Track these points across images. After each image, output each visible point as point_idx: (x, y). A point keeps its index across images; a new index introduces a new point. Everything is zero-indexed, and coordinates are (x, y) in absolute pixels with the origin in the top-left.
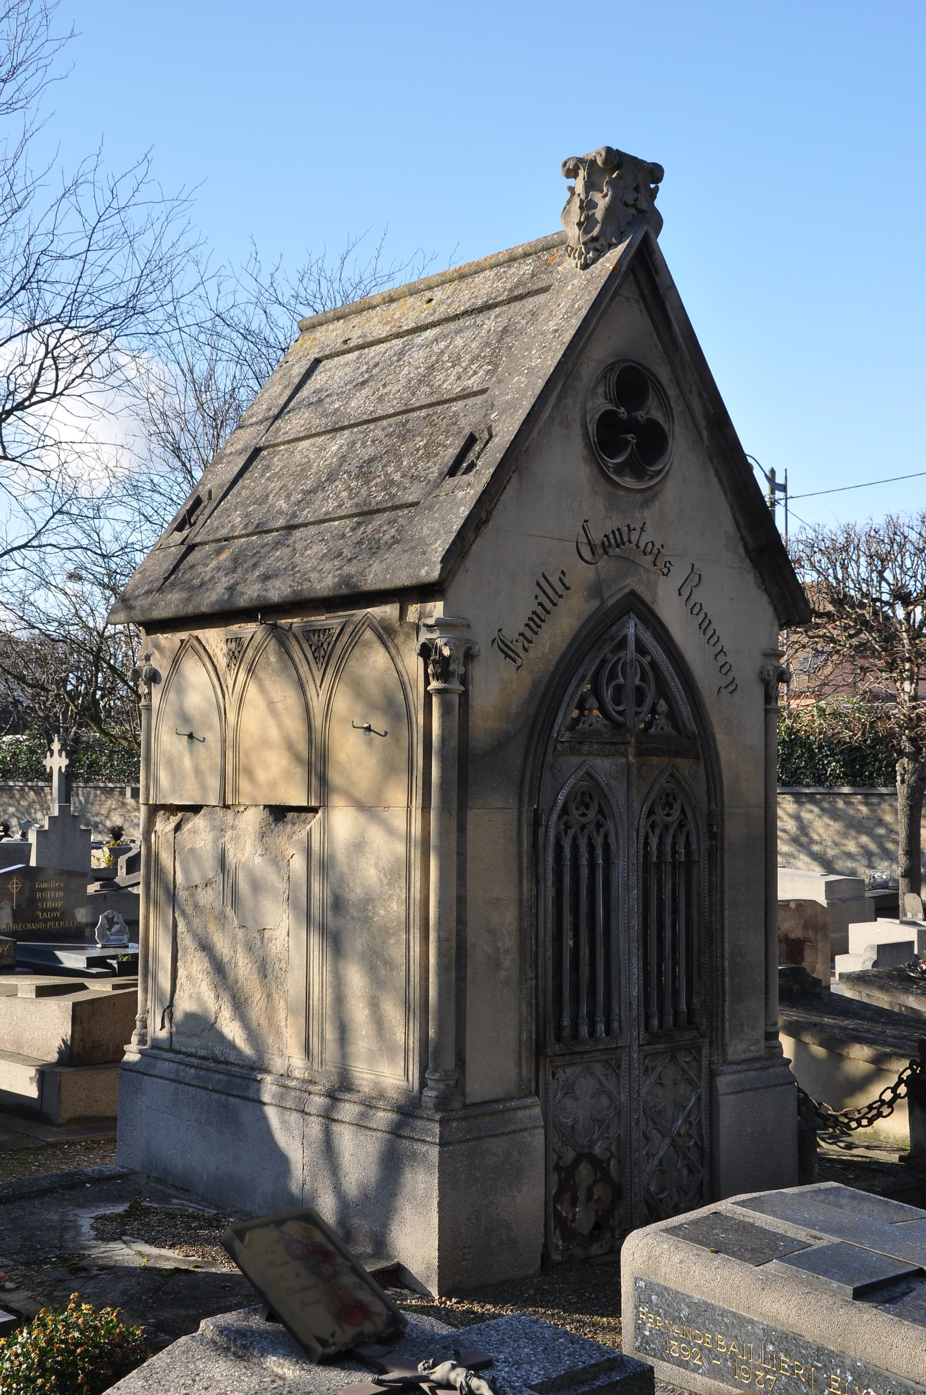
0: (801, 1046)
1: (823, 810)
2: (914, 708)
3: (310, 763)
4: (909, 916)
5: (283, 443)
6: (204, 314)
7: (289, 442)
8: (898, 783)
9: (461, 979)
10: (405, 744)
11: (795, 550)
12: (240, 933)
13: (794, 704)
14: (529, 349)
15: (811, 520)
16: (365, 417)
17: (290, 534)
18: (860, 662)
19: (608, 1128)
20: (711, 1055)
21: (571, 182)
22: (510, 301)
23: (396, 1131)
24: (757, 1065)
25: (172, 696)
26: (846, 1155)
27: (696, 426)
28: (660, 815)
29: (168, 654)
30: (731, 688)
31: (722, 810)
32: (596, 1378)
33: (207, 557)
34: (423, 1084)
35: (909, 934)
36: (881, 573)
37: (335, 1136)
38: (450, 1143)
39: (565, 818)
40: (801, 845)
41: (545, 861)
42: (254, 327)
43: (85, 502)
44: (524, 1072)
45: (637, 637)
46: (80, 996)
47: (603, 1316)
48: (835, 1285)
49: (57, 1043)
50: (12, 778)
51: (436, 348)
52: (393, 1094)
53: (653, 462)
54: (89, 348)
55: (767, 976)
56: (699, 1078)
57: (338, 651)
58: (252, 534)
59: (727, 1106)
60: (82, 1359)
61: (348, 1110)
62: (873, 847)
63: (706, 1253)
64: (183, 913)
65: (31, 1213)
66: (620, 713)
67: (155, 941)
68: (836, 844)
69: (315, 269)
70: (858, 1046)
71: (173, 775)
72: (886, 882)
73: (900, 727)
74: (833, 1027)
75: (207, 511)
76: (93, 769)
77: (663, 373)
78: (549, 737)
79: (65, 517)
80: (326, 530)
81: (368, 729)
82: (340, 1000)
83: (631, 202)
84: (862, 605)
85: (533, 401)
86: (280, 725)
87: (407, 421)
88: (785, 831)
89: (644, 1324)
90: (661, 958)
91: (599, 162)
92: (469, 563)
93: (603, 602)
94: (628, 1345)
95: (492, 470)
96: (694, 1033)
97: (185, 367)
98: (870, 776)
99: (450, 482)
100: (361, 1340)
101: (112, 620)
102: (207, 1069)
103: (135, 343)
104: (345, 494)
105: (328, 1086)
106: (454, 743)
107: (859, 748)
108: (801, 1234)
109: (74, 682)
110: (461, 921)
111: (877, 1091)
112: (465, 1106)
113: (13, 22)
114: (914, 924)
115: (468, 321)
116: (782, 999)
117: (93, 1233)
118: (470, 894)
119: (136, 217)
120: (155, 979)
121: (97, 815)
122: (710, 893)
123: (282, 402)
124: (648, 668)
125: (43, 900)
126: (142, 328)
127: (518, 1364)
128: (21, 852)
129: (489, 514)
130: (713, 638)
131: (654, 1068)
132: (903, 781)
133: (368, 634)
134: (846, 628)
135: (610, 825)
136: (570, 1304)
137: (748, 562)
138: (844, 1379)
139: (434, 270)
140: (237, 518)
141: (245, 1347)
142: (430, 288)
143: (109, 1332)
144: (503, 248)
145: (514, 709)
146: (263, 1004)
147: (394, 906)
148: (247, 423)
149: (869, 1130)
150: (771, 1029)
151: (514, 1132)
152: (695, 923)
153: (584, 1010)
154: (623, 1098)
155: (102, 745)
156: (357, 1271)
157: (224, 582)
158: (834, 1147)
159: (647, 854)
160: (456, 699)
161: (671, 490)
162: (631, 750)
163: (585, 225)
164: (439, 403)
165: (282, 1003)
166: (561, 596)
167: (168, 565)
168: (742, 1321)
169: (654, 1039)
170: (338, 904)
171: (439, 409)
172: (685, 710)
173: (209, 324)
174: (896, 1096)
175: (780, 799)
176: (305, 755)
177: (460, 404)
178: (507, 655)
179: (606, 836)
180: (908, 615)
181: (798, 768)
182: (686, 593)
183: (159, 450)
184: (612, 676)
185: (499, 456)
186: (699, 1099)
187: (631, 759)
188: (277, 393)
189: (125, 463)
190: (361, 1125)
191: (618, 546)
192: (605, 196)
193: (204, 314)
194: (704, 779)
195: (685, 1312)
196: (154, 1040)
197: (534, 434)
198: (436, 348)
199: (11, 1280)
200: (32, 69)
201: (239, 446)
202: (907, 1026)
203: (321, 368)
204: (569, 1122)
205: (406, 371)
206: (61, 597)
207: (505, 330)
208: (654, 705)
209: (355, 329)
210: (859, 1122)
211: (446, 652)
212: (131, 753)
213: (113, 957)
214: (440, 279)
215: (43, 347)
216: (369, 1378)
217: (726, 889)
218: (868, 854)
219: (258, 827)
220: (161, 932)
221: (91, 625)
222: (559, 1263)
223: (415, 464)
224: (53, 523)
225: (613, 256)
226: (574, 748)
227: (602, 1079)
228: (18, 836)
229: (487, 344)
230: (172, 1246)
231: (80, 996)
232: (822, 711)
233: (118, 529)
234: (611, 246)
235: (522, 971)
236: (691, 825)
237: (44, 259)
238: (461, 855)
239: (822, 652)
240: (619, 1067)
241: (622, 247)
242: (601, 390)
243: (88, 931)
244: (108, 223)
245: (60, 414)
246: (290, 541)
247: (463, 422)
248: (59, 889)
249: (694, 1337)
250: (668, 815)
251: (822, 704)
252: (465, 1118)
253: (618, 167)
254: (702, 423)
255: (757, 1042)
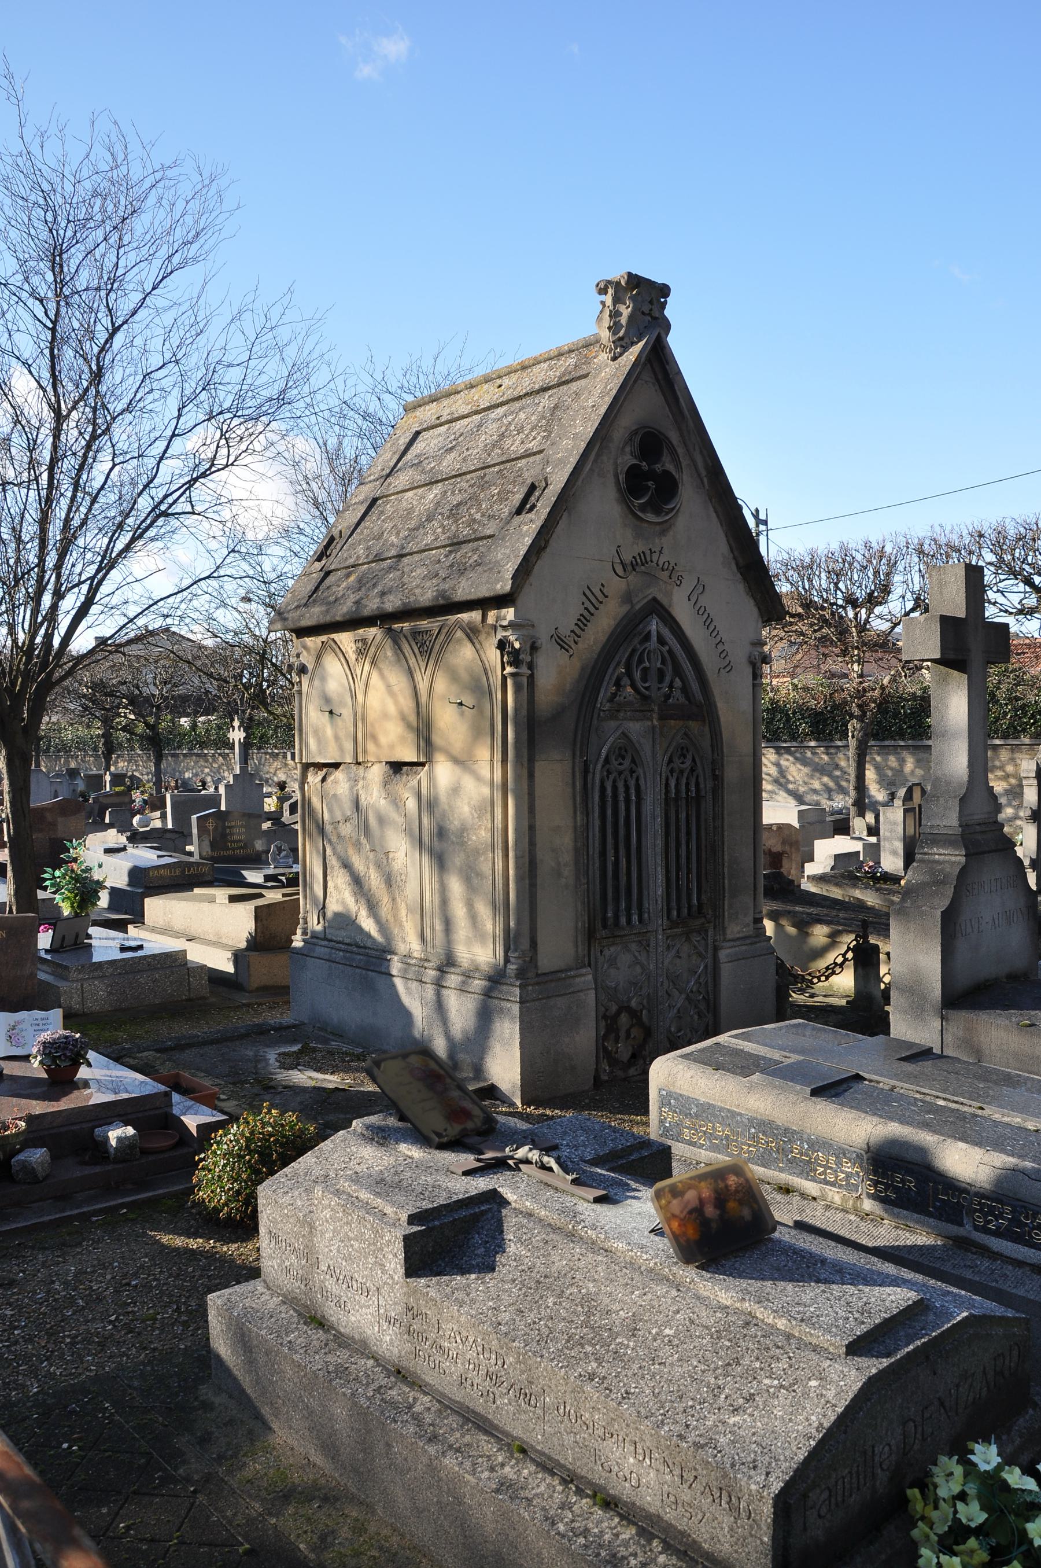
0: (779, 927)
1: (796, 758)
2: (861, 683)
3: (418, 730)
4: (857, 834)
5: (394, 494)
6: (334, 402)
7: (398, 493)
8: (850, 738)
9: (533, 885)
10: (488, 713)
11: (774, 568)
12: (371, 855)
13: (775, 682)
14: (574, 420)
15: (786, 546)
16: (454, 473)
17: (399, 561)
18: (822, 650)
19: (641, 988)
20: (715, 935)
21: (603, 298)
22: (560, 384)
23: (487, 994)
24: (748, 941)
25: (316, 683)
26: (810, 1002)
27: (699, 475)
28: (677, 764)
29: (313, 652)
30: (728, 669)
31: (722, 759)
32: (631, 1154)
33: (340, 579)
34: (507, 960)
35: (857, 846)
36: (836, 584)
37: (445, 998)
38: (528, 1002)
39: (607, 766)
40: (780, 785)
41: (593, 798)
42: (371, 410)
43: (251, 543)
44: (580, 950)
45: (658, 632)
46: (260, 902)
47: (637, 1115)
48: (798, 1087)
49: (245, 935)
50: (206, 748)
51: (505, 421)
52: (485, 968)
53: (667, 502)
54: (251, 431)
55: (755, 878)
56: (706, 952)
57: (437, 647)
58: (372, 562)
59: (726, 971)
60: (275, 1145)
61: (453, 980)
62: (832, 784)
63: (709, 1070)
64: (330, 842)
65: (234, 1050)
66: (646, 688)
67: (311, 862)
68: (806, 783)
69: (414, 367)
70: (819, 926)
71: (319, 741)
72: (841, 810)
73: (851, 697)
74: (802, 913)
75: (339, 546)
76: (264, 740)
77: (674, 436)
78: (595, 707)
79: (237, 555)
80: (426, 557)
81: (461, 704)
82: (444, 902)
83: (647, 312)
84: (823, 608)
85: (578, 458)
86: (396, 703)
87: (485, 475)
88: (769, 775)
89: (665, 1119)
90: (678, 869)
91: (623, 283)
92: (532, 579)
93: (632, 607)
94: (654, 1132)
95: (548, 510)
96: (703, 920)
97: (321, 442)
98: (830, 734)
99: (517, 519)
100: (464, 1133)
101: (272, 628)
102: (352, 952)
103: (283, 426)
104: (440, 530)
105: (439, 963)
106: (524, 712)
107: (822, 713)
108: (776, 1055)
109: (247, 676)
110: (532, 843)
111: (833, 957)
112: (538, 975)
113: (197, 201)
114: (860, 839)
115: (528, 401)
116: (766, 895)
117: (278, 1064)
118: (538, 824)
119: (284, 334)
120: (312, 889)
121: (268, 773)
122: (714, 819)
123: (392, 464)
124: (666, 655)
125: (231, 834)
126: (288, 415)
127: (576, 1147)
128: (215, 800)
129: (547, 542)
130: (714, 632)
131: (673, 946)
132: (853, 737)
133: (459, 634)
134: (812, 625)
135: (640, 771)
136: (615, 1108)
137: (739, 575)
138: (802, 1147)
139: (502, 364)
140: (361, 551)
141: (384, 1138)
142: (500, 377)
143: (292, 1128)
144: (554, 347)
145: (568, 687)
146: (389, 906)
147: (483, 833)
148: (367, 480)
149: (826, 984)
150: (758, 916)
151: (573, 992)
152: (703, 842)
153: (623, 905)
154: (651, 967)
155: (269, 722)
156: (461, 1088)
157: (353, 598)
158: (802, 997)
159: (667, 792)
160: (525, 680)
161: (681, 522)
162: (655, 716)
163: (614, 328)
164: (508, 461)
165: (403, 905)
166: (601, 603)
167: (311, 587)
168: (734, 1114)
169: (673, 925)
170: (441, 833)
171: (508, 465)
172: (695, 686)
173: (337, 409)
174: (846, 960)
175: (764, 751)
176: (415, 724)
177: (524, 461)
178: (562, 647)
179: (637, 779)
180: (856, 614)
181: (779, 728)
182: (693, 599)
183: (302, 504)
184: (640, 661)
185: (554, 499)
186: (706, 967)
187: (655, 722)
188: (388, 457)
189: (279, 513)
190: (462, 990)
191: (643, 565)
192: (628, 307)
193: (334, 402)
194: (709, 736)
195: (694, 1110)
196: (313, 932)
197: (579, 483)
198: (505, 421)
199: (224, 1094)
200: (210, 233)
201: (361, 498)
202: (853, 911)
203: (420, 438)
204: (613, 984)
205: (483, 438)
206: (236, 614)
207: (556, 407)
208: (672, 682)
209: (445, 409)
210: (819, 978)
211: (517, 645)
212: (290, 727)
213: (283, 875)
214: (507, 370)
215: (219, 431)
216: (471, 1157)
217: (726, 816)
218: (829, 790)
219: (382, 778)
220: (314, 855)
221: (258, 633)
222: (607, 1081)
223: (491, 507)
224: (228, 560)
225: (635, 350)
226: (613, 714)
227: (637, 954)
228: (212, 790)
229: (543, 417)
230: (332, 1073)
231: (260, 902)
232: (795, 686)
233: (275, 563)
234: (633, 344)
235: (577, 878)
236: (700, 770)
237: (219, 367)
238: (531, 794)
239: (795, 643)
240: (648, 945)
241: (641, 344)
242: (628, 449)
243: (264, 856)
244: (264, 339)
245: (232, 479)
246: (400, 567)
247: (526, 475)
248: (242, 826)
249: (700, 1126)
250: (683, 763)
251: (795, 681)
252: (538, 984)
253: (637, 286)
254: (703, 473)
255: (748, 925)
